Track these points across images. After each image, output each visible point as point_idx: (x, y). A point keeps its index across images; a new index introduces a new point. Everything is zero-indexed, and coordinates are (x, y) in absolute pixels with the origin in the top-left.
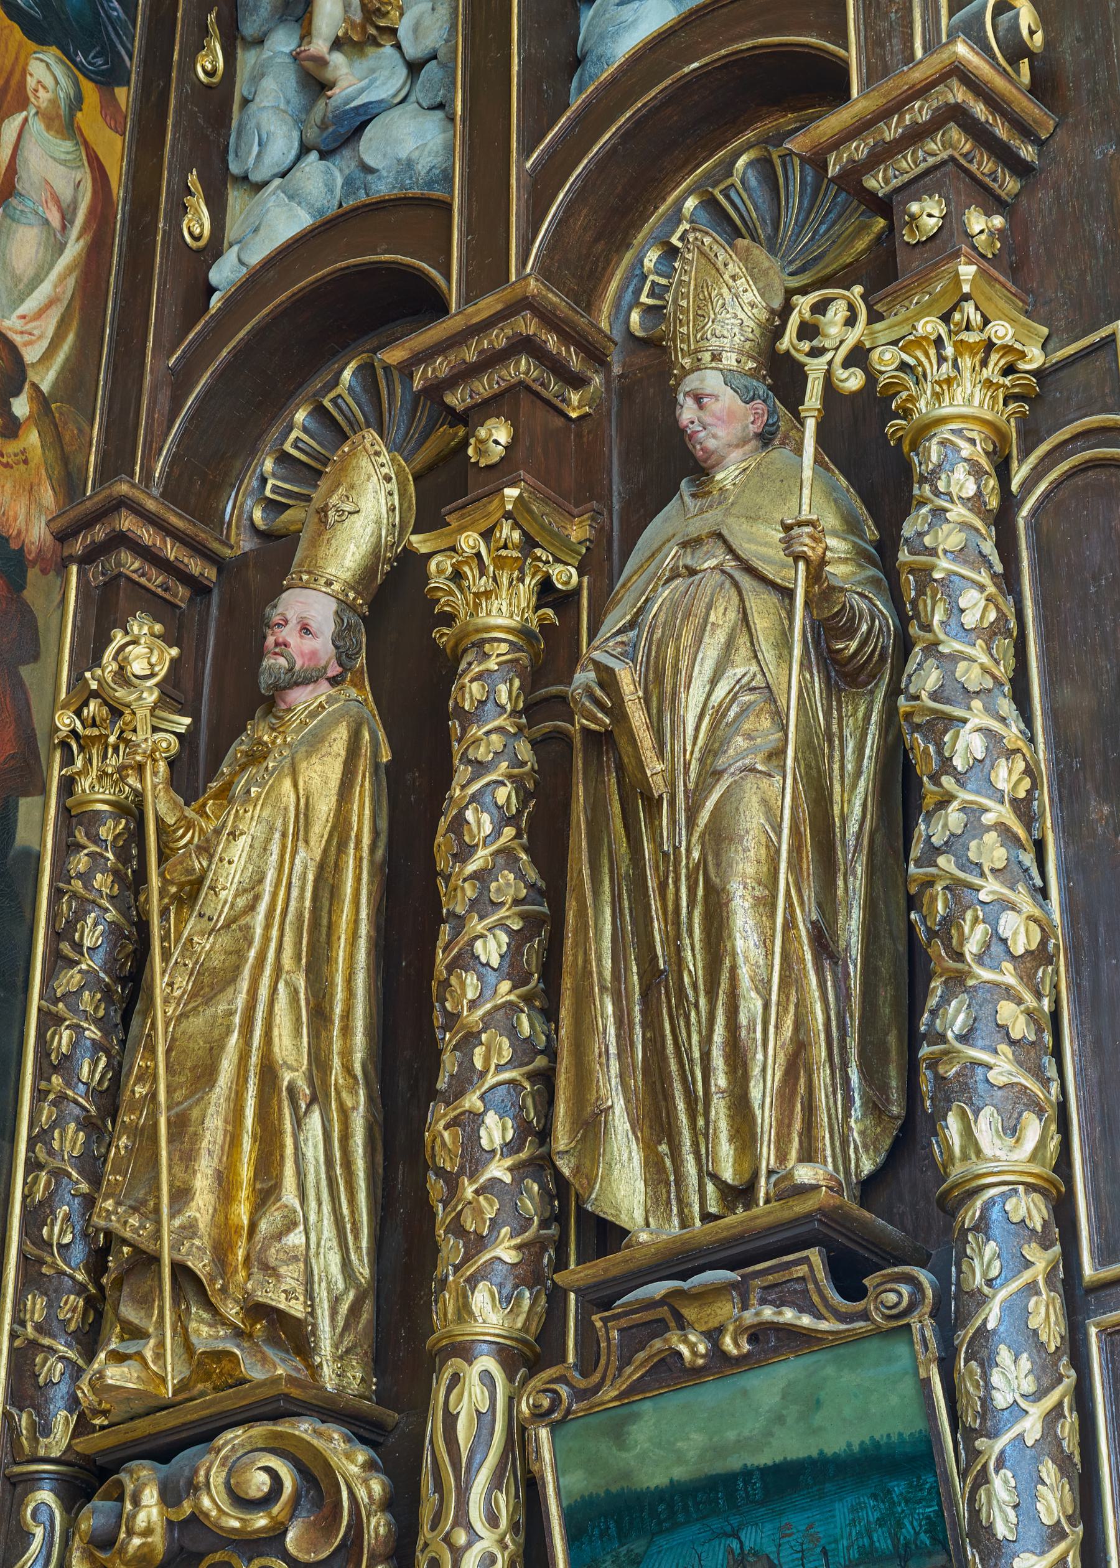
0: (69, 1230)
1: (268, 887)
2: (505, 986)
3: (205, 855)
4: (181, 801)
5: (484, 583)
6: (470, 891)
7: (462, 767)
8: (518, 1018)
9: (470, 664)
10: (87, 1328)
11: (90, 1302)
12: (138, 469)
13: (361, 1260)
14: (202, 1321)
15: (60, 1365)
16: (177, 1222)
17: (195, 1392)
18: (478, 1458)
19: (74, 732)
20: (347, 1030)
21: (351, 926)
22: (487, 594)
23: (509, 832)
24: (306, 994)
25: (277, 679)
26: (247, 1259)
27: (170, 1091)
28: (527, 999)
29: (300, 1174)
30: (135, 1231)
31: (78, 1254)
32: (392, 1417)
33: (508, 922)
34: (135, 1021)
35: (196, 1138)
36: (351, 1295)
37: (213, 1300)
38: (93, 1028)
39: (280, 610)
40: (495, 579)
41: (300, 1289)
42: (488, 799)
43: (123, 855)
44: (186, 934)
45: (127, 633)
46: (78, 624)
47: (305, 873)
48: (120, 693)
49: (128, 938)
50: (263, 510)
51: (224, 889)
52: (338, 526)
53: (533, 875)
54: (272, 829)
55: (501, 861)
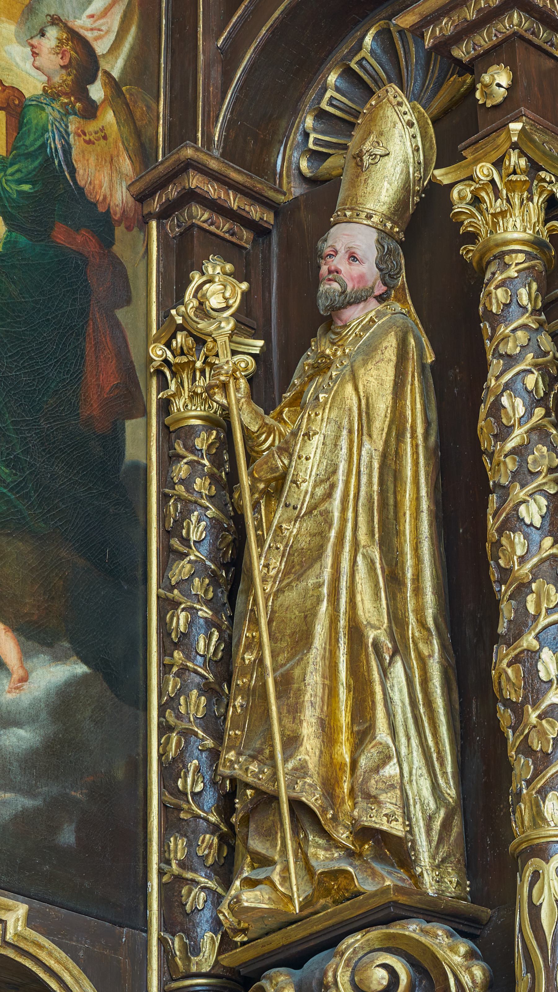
0: (200, 780)
1: (341, 476)
4: (262, 411)
6: (511, 465)
7: (495, 361)
9: (494, 274)
11: (223, 839)
12: (199, 135)
13: (447, 783)
14: (319, 846)
15: (203, 894)
16: (290, 765)
17: (318, 906)
20: (418, 591)
21: (414, 503)
22: (503, 214)
23: (539, 412)
24: (381, 563)
25: (333, 301)
26: (352, 790)
27: (274, 655)
30: (255, 775)
31: (209, 799)
32: (485, 912)
33: (545, 488)
34: (240, 599)
35: (300, 693)
37: (326, 828)
38: (204, 608)
39: (330, 242)
40: (508, 201)
41: (399, 812)
42: (519, 386)
43: (216, 461)
44: (275, 522)
45: (203, 274)
46: (162, 270)
48: (202, 325)
51: (304, 481)
52: (373, 168)
54: (340, 428)
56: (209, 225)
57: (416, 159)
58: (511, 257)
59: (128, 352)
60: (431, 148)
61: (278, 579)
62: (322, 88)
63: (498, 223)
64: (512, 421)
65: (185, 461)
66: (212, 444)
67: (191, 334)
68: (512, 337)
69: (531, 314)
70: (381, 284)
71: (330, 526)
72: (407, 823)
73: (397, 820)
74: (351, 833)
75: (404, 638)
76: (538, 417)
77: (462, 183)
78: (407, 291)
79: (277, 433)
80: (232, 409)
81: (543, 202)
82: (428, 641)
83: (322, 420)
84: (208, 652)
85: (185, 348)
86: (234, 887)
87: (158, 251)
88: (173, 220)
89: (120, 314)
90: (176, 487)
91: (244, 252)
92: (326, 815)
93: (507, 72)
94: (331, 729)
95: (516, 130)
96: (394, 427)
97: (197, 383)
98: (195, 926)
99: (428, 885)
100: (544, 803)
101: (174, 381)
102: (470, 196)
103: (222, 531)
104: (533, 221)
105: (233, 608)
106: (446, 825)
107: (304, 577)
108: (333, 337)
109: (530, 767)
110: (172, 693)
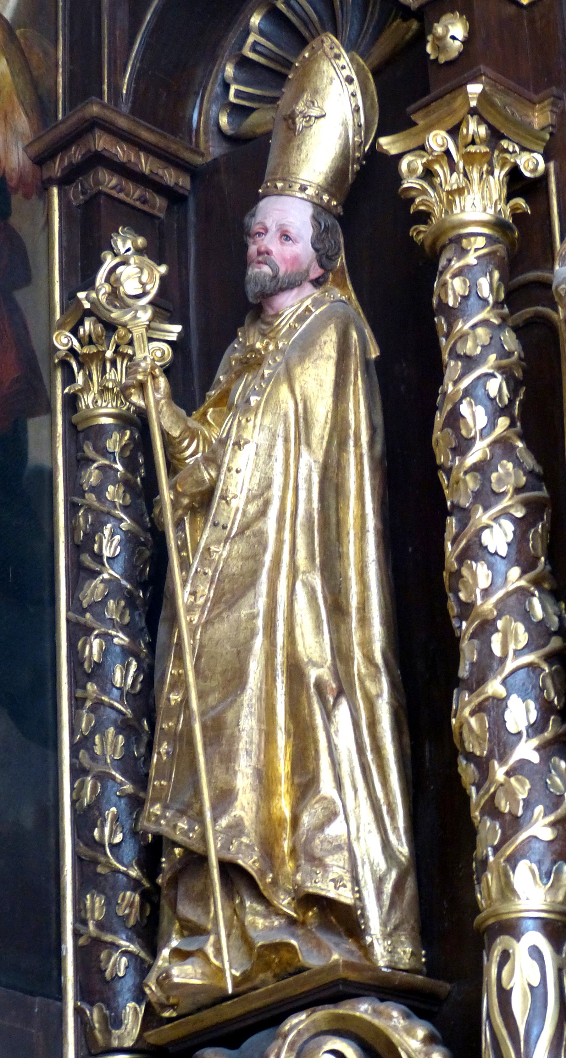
0: (119, 830)
1: (276, 492)
2: (515, 572)
3: (213, 466)
4: (183, 412)
5: (455, 180)
6: (472, 483)
7: (452, 363)
8: (531, 603)
9: (450, 261)
10: (145, 921)
11: (145, 896)
12: (105, 88)
13: (399, 839)
14: (256, 913)
15: (124, 960)
16: (224, 822)
17: (257, 982)
18: (535, 1031)
19: (72, 351)
20: (364, 621)
21: (358, 520)
22: (460, 191)
23: (503, 422)
24: (323, 592)
25: (263, 287)
26: (293, 851)
27: (201, 696)
28: (536, 583)
29: (335, 765)
30: (185, 833)
31: (129, 851)
32: (443, 987)
33: (512, 511)
34: (162, 629)
35: (234, 739)
36: (394, 875)
37: (265, 894)
38: (120, 635)
39: (259, 218)
40: (465, 175)
41: (347, 877)
42: (480, 392)
43: (130, 464)
44: (202, 544)
45: (116, 255)
46: (65, 244)
47: (310, 476)
48: (115, 314)
49: (143, 544)
50: (229, 116)
51: (235, 497)
52: (307, 132)
53: (530, 462)
54: (274, 436)
55: (499, 451)
56: (118, 192)
57: (356, 121)
58: (470, 241)
59: (28, 340)
60: (372, 106)
61: (207, 609)
62: (243, 31)
63: (454, 201)
64: (473, 434)
65: (95, 465)
66: (126, 445)
67: (100, 320)
68: (471, 335)
69: (493, 307)
70: (317, 266)
71: (265, 549)
72: (356, 889)
73: (345, 886)
74: (293, 899)
75: (350, 674)
76: (502, 427)
77: (412, 153)
78: (347, 275)
79: (201, 438)
80: (151, 413)
81: (505, 176)
82: (376, 679)
83: (254, 427)
84: (125, 684)
85: (94, 337)
86: (162, 957)
87: (60, 222)
88: (76, 187)
89: (20, 296)
90: (86, 495)
91: (157, 222)
92: (265, 879)
93: (462, 23)
94: (268, 780)
95: (475, 93)
96: (335, 434)
97: (107, 375)
98: (116, 994)
99: (379, 957)
100: (514, 872)
101: (81, 374)
102: (420, 169)
103: (138, 546)
104: (494, 199)
105: (153, 633)
106: (398, 887)
107: (236, 606)
108: (264, 327)
109: (496, 832)
110: (86, 731)
